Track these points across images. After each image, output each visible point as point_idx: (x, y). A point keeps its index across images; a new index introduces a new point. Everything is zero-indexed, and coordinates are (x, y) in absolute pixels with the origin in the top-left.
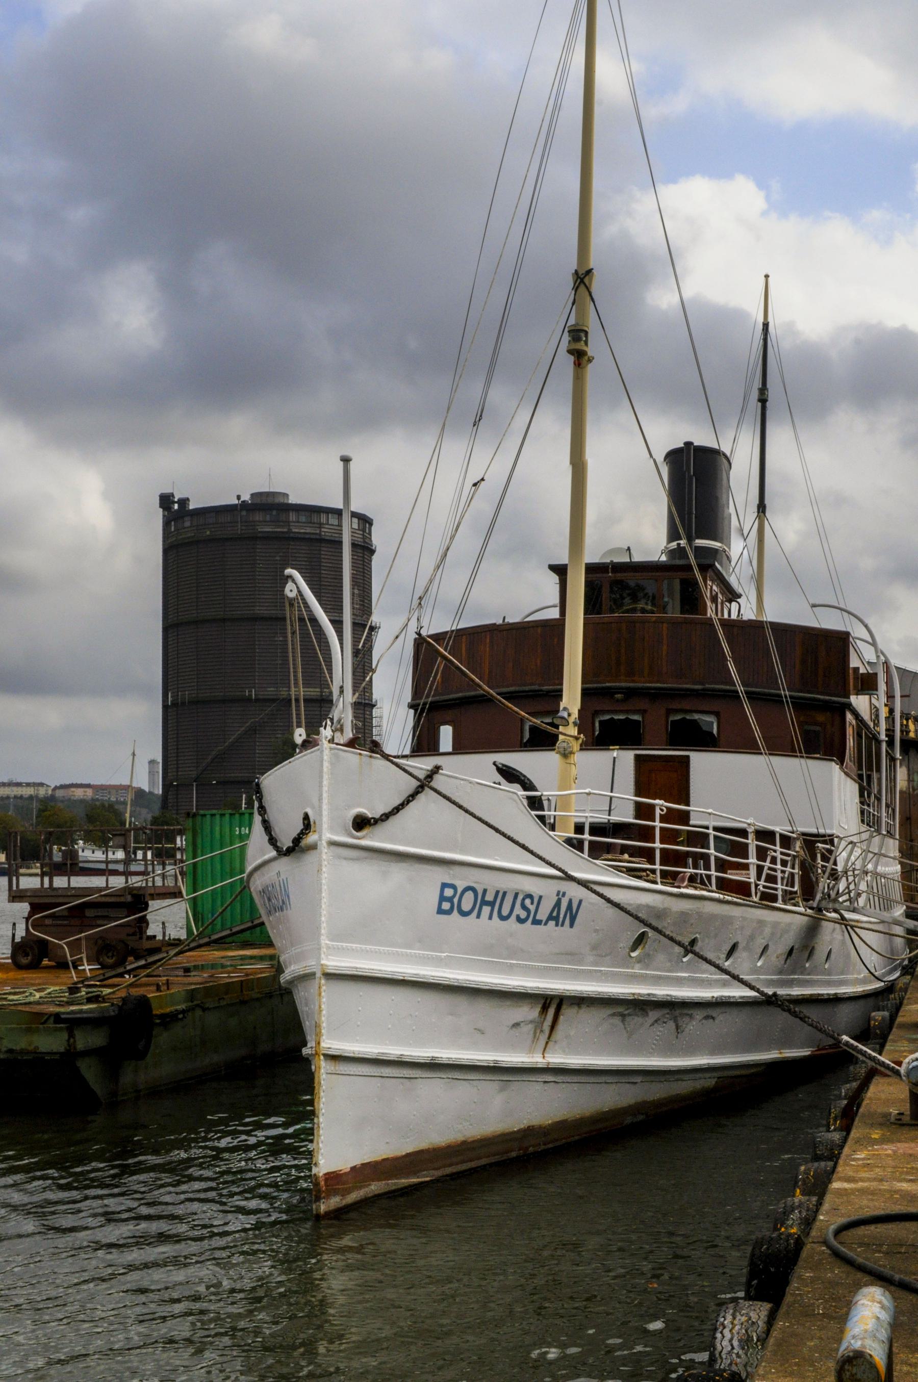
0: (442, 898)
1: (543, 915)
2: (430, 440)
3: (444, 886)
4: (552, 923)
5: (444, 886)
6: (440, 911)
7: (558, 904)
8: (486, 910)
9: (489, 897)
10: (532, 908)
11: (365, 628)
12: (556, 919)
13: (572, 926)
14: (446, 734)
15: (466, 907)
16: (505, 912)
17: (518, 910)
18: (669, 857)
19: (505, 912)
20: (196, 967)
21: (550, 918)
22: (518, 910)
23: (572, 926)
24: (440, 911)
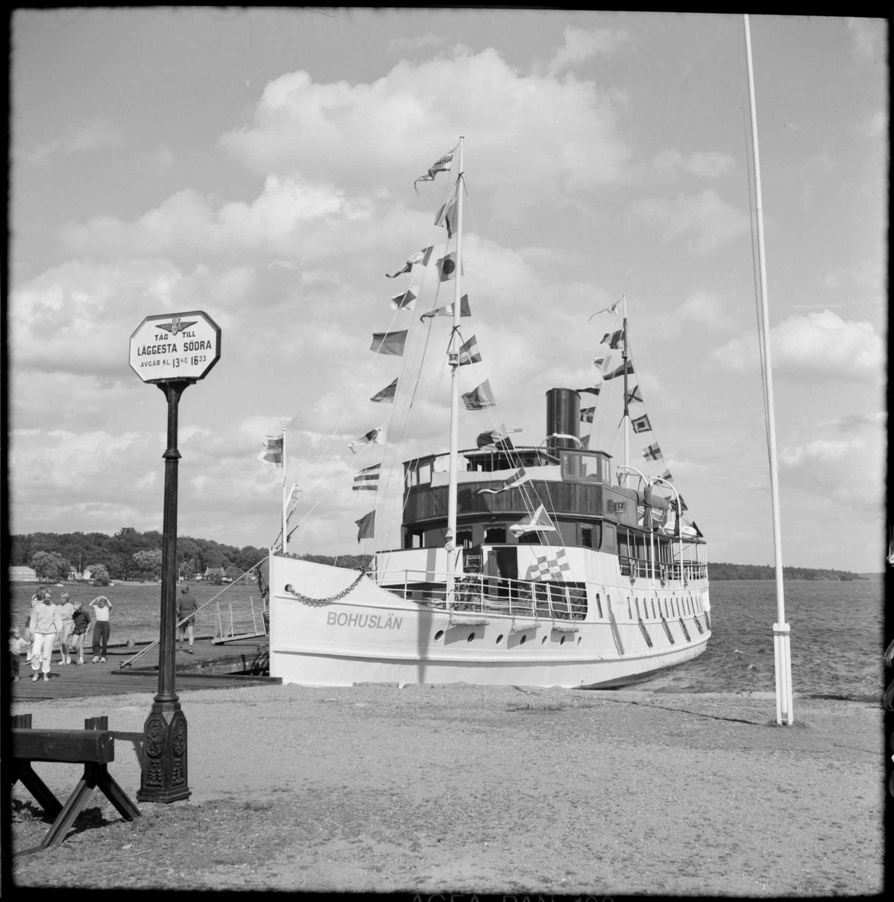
0: (329, 618)
1: (382, 624)
2: (17, 615)
3: (330, 613)
4: (388, 627)
5: (330, 613)
6: (328, 623)
7: (390, 619)
8: (352, 623)
9: (354, 617)
10: (377, 621)
11: (569, 433)
12: (390, 625)
13: (399, 627)
14: (416, 539)
15: (342, 622)
16: (362, 623)
17: (369, 622)
18: (515, 594)
19: (362, 623)
20: (468, 363)
21: (387, 625)
22: (369, 622)
23: (399, 627)
24: (328, 623)
